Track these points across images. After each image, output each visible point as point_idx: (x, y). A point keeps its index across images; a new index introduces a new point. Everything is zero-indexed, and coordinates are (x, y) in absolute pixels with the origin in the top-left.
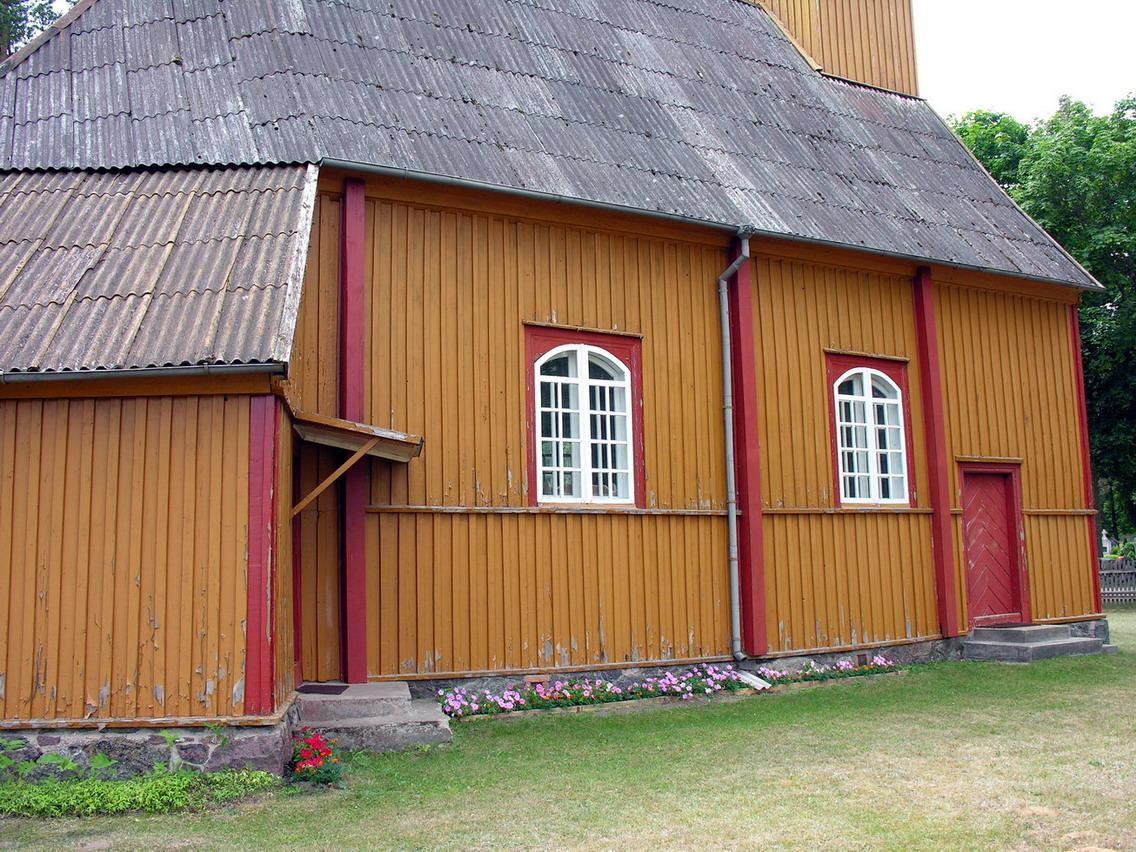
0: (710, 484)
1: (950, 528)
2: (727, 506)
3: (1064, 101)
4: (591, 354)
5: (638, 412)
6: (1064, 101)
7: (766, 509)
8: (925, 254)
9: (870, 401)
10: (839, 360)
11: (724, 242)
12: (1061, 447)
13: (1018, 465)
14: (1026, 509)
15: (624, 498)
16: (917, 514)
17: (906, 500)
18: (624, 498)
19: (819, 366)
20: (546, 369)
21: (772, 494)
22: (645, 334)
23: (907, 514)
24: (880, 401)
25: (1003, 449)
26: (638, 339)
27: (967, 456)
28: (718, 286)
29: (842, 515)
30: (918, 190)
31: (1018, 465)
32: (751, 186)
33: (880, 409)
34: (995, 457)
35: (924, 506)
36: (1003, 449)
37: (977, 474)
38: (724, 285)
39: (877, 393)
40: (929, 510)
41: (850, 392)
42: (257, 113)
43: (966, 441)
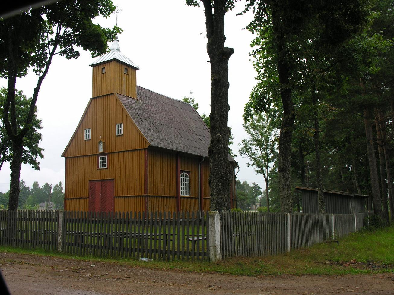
15: (188, 195)
20: (181, 176)
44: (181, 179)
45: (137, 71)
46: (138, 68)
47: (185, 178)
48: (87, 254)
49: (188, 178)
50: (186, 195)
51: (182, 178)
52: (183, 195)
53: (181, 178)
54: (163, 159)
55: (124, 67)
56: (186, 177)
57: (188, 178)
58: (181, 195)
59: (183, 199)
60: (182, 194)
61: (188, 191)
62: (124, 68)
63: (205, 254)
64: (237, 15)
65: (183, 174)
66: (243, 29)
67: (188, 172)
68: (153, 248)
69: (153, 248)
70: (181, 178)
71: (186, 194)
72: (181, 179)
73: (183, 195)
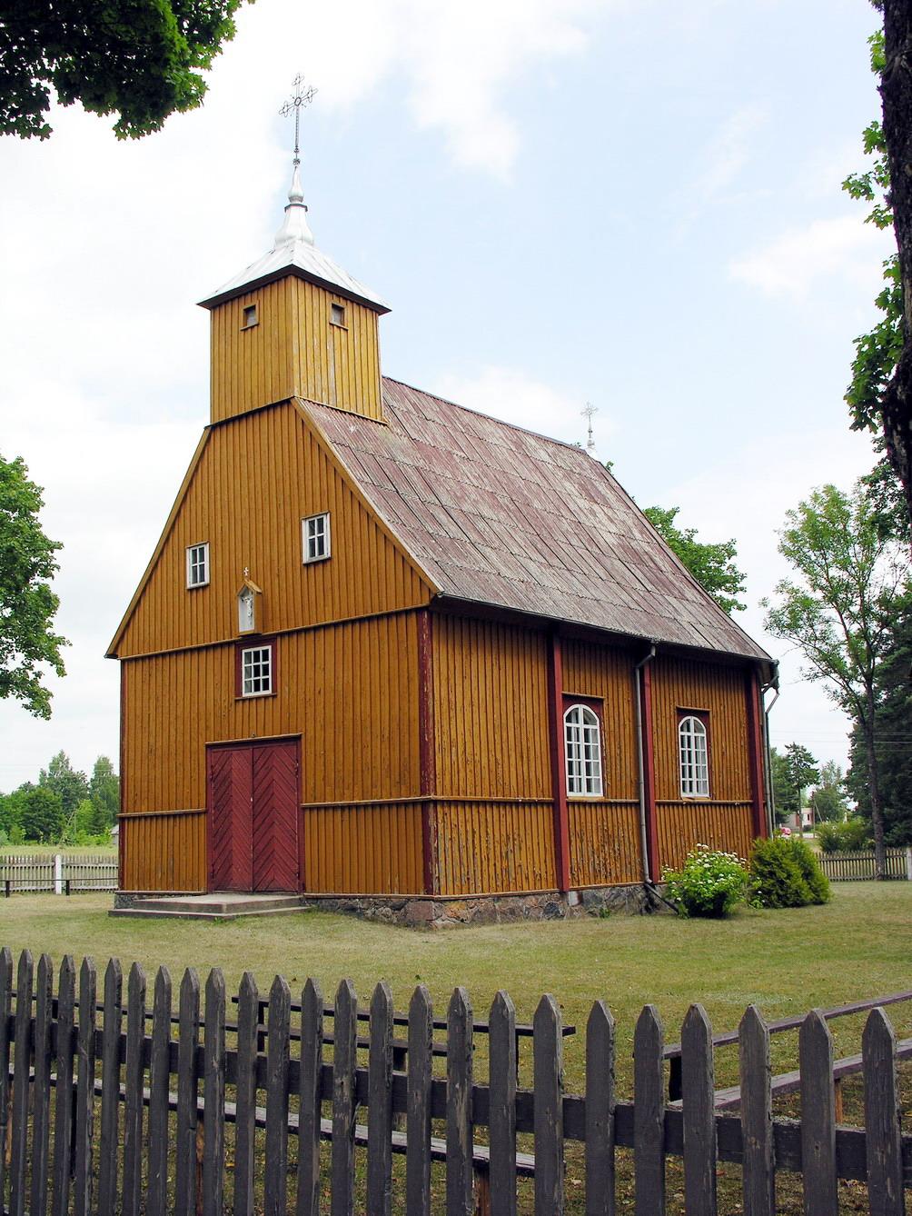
10: (682, 713)
15: (597, 795)
20: (569, 719)
26: (602, 701)
47: (582, 726)
53: (569, 725)
56: (586, 723)
57: (594, 727)
58: (569, 794)
59: (737, 810)
61: (597, 777)
65: (688, 721)
70: (681, 733)
71: (589, 789)
72: (569, 729)
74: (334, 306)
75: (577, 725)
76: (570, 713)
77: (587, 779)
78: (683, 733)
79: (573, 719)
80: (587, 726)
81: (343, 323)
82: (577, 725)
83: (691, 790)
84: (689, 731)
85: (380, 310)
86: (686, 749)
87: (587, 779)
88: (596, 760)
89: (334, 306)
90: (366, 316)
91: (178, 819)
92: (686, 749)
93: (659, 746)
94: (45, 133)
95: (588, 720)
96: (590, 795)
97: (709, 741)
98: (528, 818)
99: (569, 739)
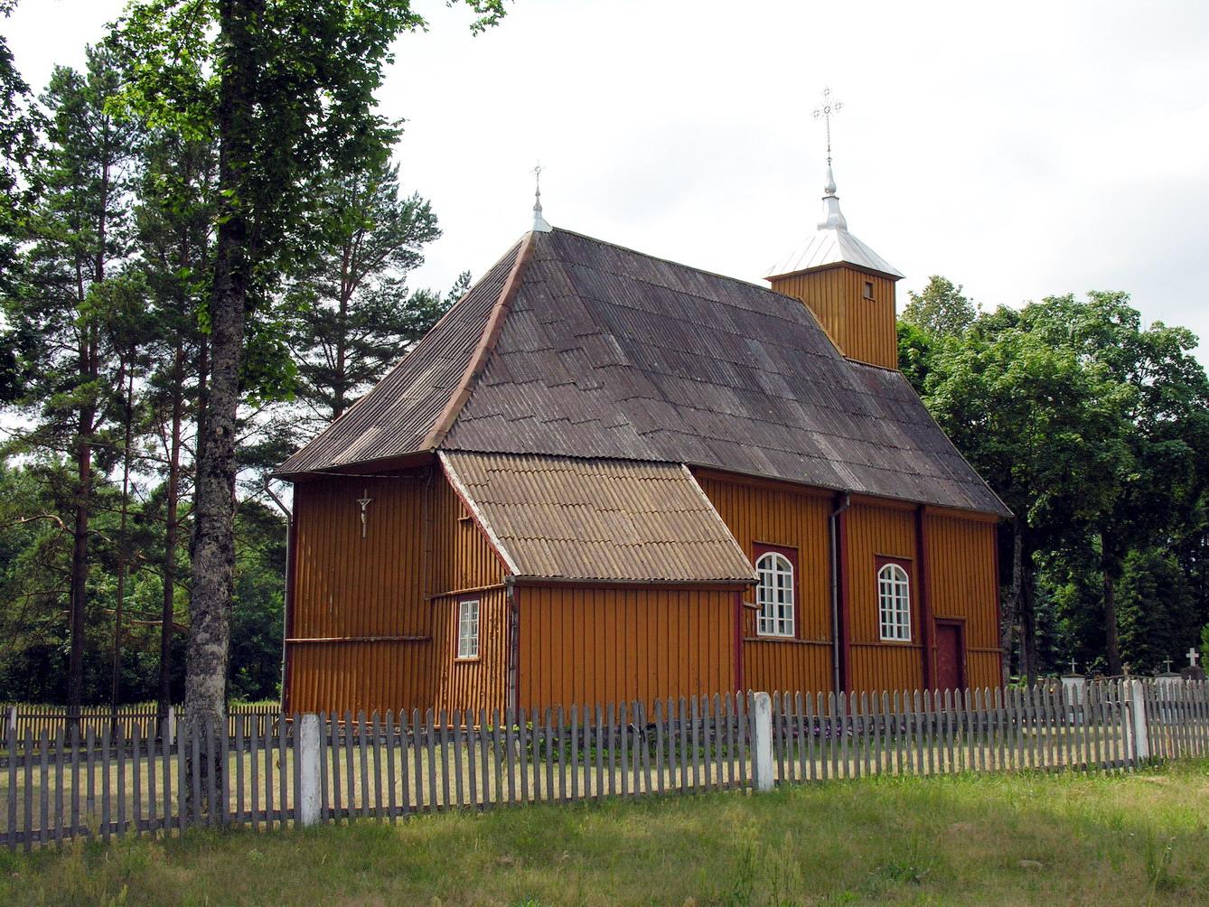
0: (825, 626)
1: (751, 724)
2: (833, 641)
3: (935, 281)
4: (778, 558)
5: (797, 588)
6: (935, 281)
7: (853, 642)
8: (923, 499)
9: (775, 572)
10: (881, 560)
11: (837, 498)
12: (403, 679)
13: (964, 621)
14: (967, 647)
15: (790, 634)
16: (915, 648)
17: (910, 640)
18: (790, 634)
19: (872, 562)
20: (882, 576)
21: (854, 636)
22: (800, 548)
23: (911, 647)
24: (781, 573)
25: (948, 613)
26: (797, 550)
27: (939, 616)
28: (830, 520)
29: (882, 646)
30: (910, 449)
31: (964, 621)
32: (840, 459)
33: (780, 577)
34: (953, 616)
35: (918, 644)
36: (948, 613)
37: (943, 625)
38: (834, 519)
39: (779, 568)
40: (921, 645)
41: (764, 568)
42: (639, 429)
43: (941, 607)
44: (883, 585)
45: (898, 283)
46: (900, 275)
47: (893, 582)
48: (305, 710)
49: (905, 583)
50: (899, 639)
51: (886, 581)
52: (891, 639)
53: (883, 581)
54: (877, 519)
55: (864, 279)
56: (897, 579)
57: (905, 583)
58: (882, 638)
59: (884, 651)
60: (884, 635)
61: (790, 619)
62: (864, 283)
63: (330, 743)
64: (538, 171)
65: (770, 558)
66: (538, 194)
67: (791, 553)
68: (594, 770)
69: (594, 770)
70: (880, 580)
71: (899, 636)
72: (883, 585)
73: (891, 639)
74: (867, 283)
75: (770, 571)
76: (763, 560)
77: (780, 621)
78: (883, 581)
79: (886, 575)
80: (898, 582)
81: (871, 296)
82: (770, 571)
83: (892, 636)
84: (890, 578)
85: (895, 278)
86: (886, 595)
87: (780, 621)
88: (789, 604)
89: (867, 283)
90: (887, 284)
91: (312, 648)
92: (886, 595)
93: (853, 587)
94: (1091, 294)
95: (782, 566)
96: (899, 639)
97: (796, 579)
98: (766, 654)
99: (883, 592)
